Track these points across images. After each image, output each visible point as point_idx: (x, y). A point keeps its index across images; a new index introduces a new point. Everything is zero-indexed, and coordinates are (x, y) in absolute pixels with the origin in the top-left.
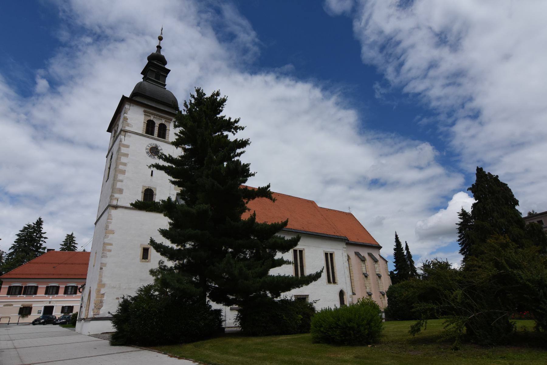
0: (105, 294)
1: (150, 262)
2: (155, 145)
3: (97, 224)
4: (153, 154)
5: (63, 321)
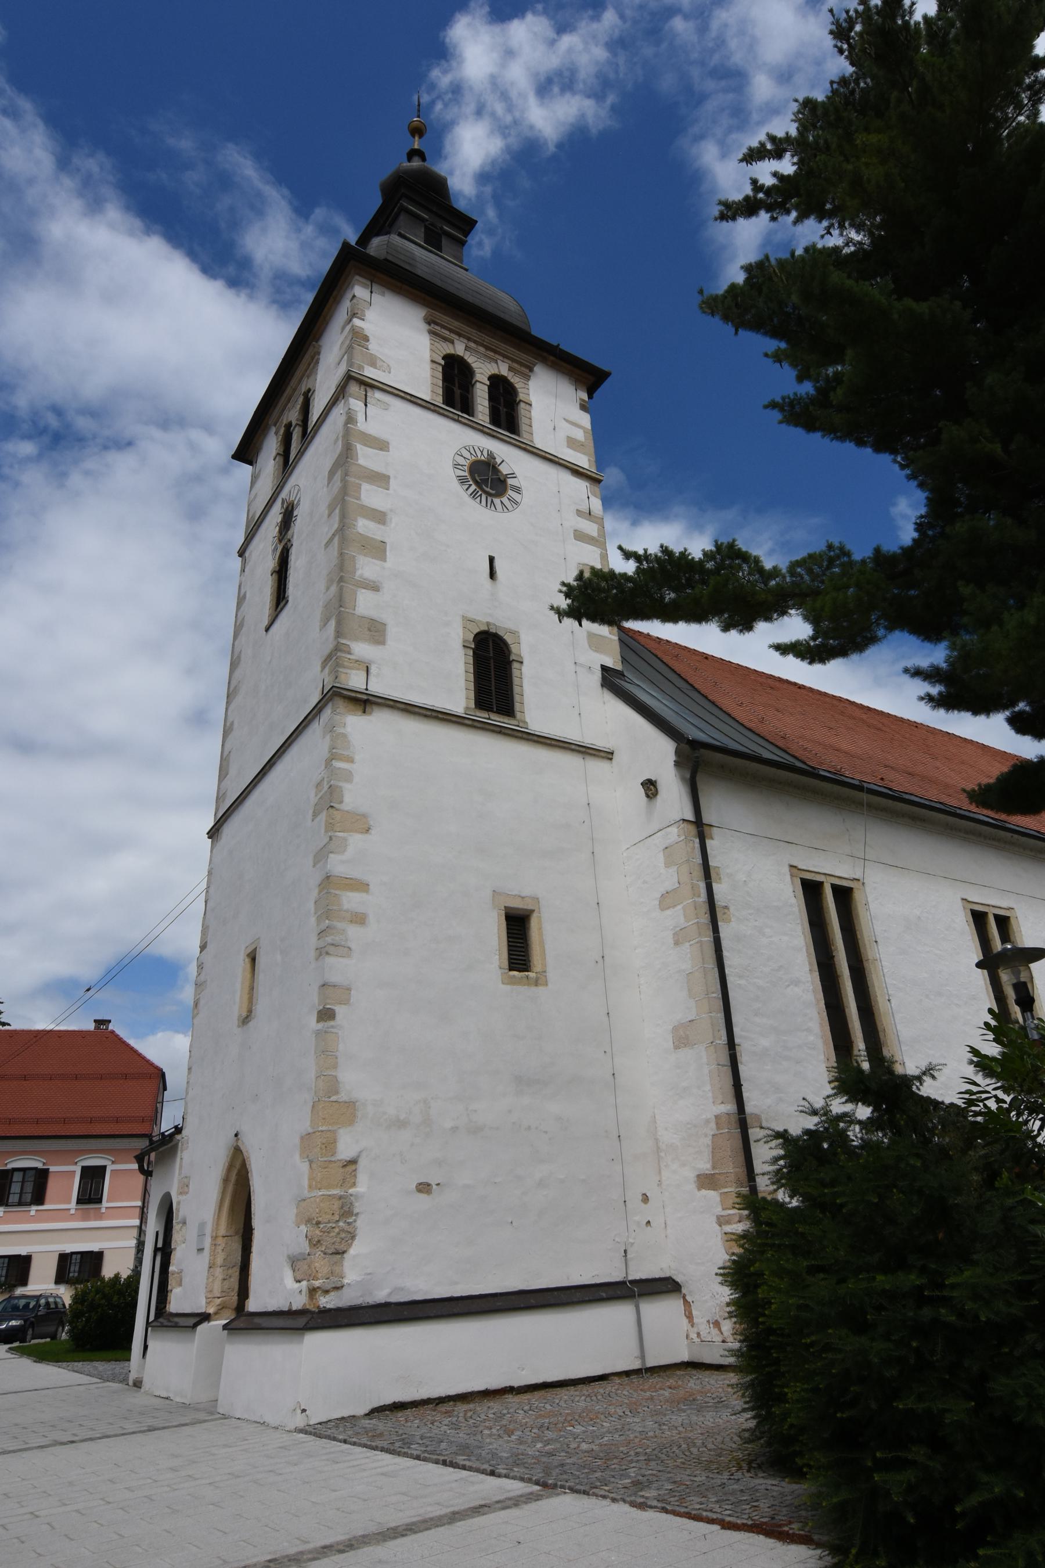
0: (362, 1163)
1: (546, 984)
2: (485, 453)
3: (227, 830)
4: (488, 490)
5: (13, 1323)
